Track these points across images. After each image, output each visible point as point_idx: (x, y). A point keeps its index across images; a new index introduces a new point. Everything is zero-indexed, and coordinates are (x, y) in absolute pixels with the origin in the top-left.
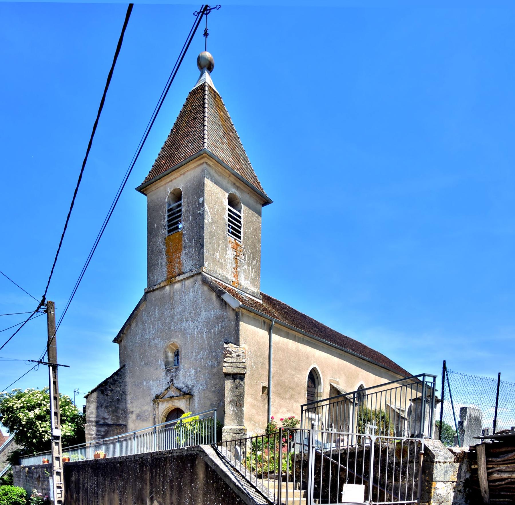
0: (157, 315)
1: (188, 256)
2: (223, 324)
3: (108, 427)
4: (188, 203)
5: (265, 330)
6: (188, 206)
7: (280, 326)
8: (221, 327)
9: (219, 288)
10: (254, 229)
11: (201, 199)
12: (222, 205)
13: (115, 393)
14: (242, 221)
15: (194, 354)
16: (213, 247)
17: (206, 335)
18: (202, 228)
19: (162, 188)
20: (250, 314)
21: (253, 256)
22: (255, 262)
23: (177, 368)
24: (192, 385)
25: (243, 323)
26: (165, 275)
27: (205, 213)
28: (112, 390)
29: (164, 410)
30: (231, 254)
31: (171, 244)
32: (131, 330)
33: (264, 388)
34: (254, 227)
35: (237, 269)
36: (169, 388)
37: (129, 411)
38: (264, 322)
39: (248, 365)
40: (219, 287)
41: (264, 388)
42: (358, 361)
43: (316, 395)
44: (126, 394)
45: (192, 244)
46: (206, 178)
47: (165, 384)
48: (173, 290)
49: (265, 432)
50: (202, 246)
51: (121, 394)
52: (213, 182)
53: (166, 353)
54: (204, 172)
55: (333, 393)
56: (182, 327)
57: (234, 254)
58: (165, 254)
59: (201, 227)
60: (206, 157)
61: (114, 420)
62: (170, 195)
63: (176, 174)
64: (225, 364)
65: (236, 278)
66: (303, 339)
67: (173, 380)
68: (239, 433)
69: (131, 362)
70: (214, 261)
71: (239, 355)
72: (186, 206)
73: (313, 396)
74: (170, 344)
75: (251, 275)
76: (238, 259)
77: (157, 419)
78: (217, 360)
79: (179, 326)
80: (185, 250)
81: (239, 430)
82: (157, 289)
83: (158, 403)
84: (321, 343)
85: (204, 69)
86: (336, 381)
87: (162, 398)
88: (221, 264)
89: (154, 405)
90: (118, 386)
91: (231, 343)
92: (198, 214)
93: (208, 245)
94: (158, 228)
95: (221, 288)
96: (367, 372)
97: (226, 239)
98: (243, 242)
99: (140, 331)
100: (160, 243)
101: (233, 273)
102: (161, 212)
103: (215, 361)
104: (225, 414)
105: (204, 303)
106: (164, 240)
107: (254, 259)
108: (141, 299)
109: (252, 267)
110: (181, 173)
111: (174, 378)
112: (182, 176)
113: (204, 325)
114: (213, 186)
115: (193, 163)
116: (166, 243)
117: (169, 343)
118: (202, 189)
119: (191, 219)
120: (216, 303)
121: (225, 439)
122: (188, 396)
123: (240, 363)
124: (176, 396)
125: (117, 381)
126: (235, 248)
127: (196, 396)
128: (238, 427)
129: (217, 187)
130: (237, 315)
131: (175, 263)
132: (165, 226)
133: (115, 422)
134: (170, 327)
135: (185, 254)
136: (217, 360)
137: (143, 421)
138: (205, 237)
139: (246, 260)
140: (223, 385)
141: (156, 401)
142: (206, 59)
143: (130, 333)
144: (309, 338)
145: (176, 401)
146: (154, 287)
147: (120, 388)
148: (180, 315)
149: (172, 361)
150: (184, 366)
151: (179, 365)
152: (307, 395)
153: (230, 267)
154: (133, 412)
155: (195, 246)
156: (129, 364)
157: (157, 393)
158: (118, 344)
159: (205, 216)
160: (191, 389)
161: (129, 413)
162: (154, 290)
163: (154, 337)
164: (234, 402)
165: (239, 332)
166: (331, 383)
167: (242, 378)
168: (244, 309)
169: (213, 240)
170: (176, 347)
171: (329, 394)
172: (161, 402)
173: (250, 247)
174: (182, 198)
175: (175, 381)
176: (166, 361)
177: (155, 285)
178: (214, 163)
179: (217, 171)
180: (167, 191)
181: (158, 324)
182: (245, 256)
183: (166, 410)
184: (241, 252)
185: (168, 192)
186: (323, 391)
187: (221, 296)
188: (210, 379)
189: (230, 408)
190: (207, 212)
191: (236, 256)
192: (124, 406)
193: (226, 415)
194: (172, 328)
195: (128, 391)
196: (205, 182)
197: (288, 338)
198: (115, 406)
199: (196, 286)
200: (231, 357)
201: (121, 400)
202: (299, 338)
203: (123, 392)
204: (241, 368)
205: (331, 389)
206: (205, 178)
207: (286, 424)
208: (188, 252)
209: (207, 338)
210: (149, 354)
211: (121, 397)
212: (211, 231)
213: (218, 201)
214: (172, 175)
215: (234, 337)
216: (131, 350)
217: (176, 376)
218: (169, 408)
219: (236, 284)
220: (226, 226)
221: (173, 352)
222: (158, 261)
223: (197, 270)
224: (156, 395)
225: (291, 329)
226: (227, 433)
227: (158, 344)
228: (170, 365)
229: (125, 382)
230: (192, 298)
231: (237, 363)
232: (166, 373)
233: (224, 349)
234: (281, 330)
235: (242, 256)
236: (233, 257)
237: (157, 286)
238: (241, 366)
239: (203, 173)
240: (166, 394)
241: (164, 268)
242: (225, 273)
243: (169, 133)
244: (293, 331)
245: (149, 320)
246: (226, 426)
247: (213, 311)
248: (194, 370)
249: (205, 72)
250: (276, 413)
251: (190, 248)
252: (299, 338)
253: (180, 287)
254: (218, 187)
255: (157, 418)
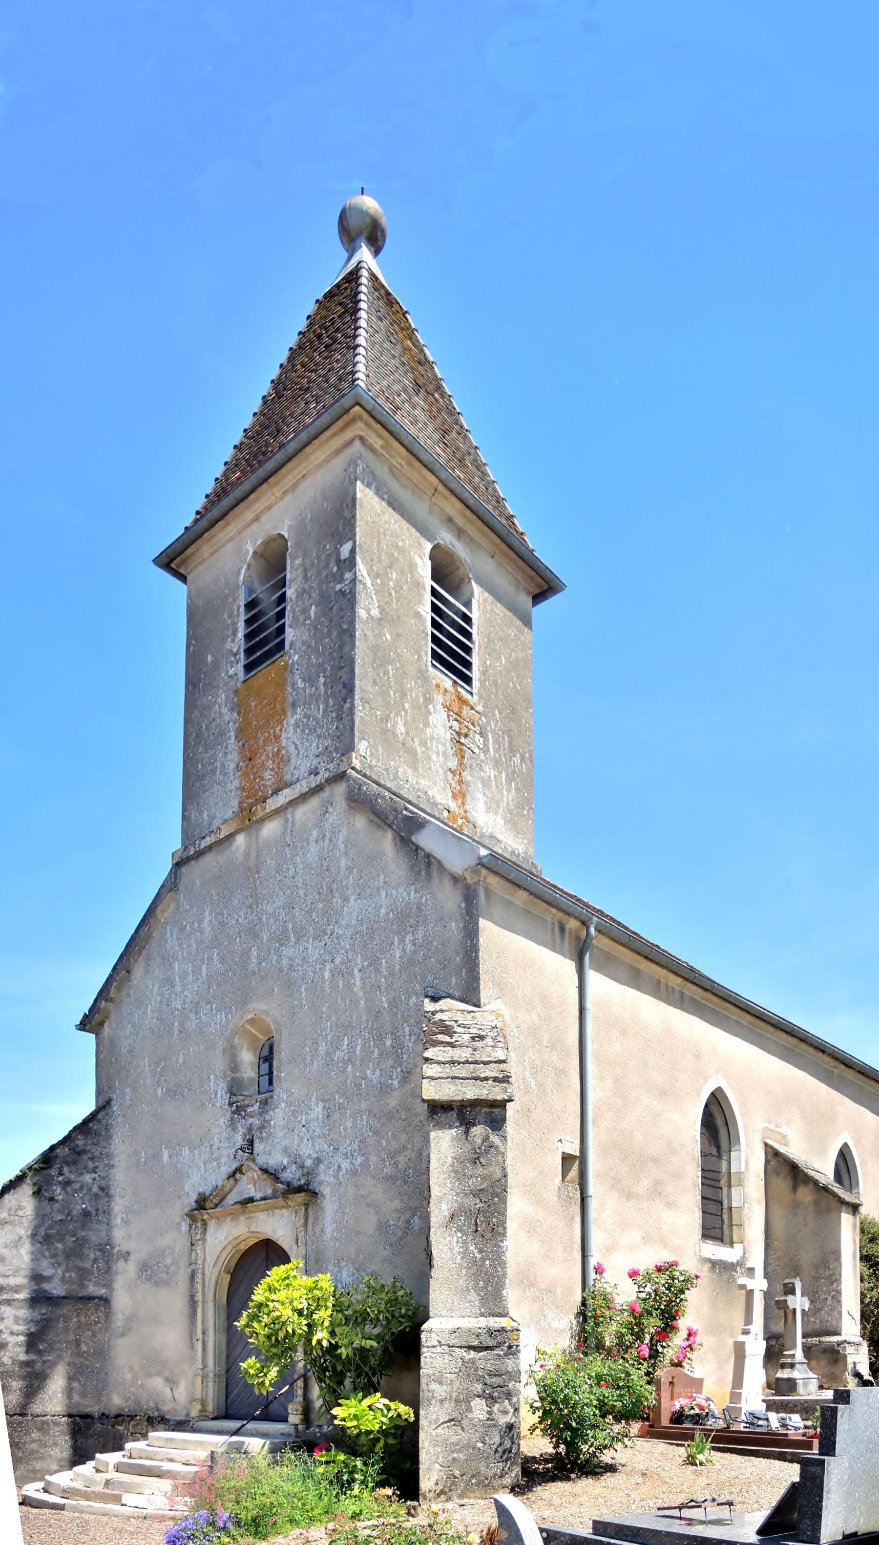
0: (207, 929)
1: (303, 731)
2: (420, 935)
3: (50, 1305)
4: (305, 570)
5: (565, 957)
6: (306, 578)
7: (611, 943)
8: (414, 944)
9: (405, 812)
10: (511, 663)
11: (344, 546)
12: (412, 573)
13: (76, 1191)
14: (474, 631)
15: (322, 1049)
16: (384, 694)
17: (362, 979)
18: (347, 634)
19: (229, 546)
20: (513, 895)
21: (510, 743)
22: (517, 759)
23: (266, 1100)
24: (315, 1156)
25: (490, 924)
26: (235, 803)
27: (359, 587)
28: (67, 1183)
29: (225, 1248)
30: (444, 726)
31: (253, 704)
32: (130, 988)
33: (567, 1159)
34: (510, 654)
35: (463, 774)
36: (239, 1170)
37: (119, 1251)
38: (562, 929)
39: (513, 1069)
40: (406, 809)
41: (567, 1159)
42: (832, 1072)
43: (723, 1183)
44: (112, 1196)
45: (317, 689)
46: (363, 482)
47: (229, 1156)
48: (257, 843)
49: (575, 1322)
50: (349, 688)
51: (96, 1195)
52: (383, 499)
53: (231, 1053)
54: (356, 466)
55: (778, 1174)
56: (285, 962)
57: (451, 727)
58: (236, 737)
59: (346, 631)
60: (361, 419)
61: (70, 1281)
62: (253, 563)
63: (269, 494)
64: (430, 1070)
65: (460, 801)
66: (682, 994)
67: (251, 1142)
68: (487, 1348)
69: (128, 1090)
70: (388, 737)
71: (482, 1038)
72: (300, 578)
73: (713, 1183)
74: (245, 1020)
75: (505, 799)
76: (463, 744)
77: (199, 1279)
78: (401, 1065)
79: (275, 958)
80: (294, 713)
81: (491, 1332)
82: (210, 848)
83: (205, 1223)
84: (733, 1008)
85: (358, 241)
86: (780, 1133)
87: (216, 1206)
88: (412, 752)
89: (193, 1231)
90: (85, 1168)
91: (450, 996)
92: (336, 593)
93: (369, 688)
94: (216, 663)
95: (410, 812)
96: (856, 1105)
97: (425, 678)
98: (481, 697)
99: (156, 988)
100: (220, 707)
101: (451, 785)
102: (226, 615)
103: (393, 1067)
104: (431, 1266)
105: (355, 871)
106: (232, 696)
107: (512, 750)
108: (162, 886)
109: (507, 775)
110: (287, 487)
111: (257, 1134)
112: (288, 498)
113: (354, 946)
114: (384, 513)
115: (321, 445)
116: (238, 705)
117: (242, 1017)
118: (350, 516)
119: (315, 614)
120: (394, 866)
121: (431, 1372)
122: (300, 1197)
123: (485, 1063)
124: (264, 1199)
125: (84, 1152)
126: (456, 710)
127: (328, 1198)
128: (484, 1322)
129: (397, 516)
130: (469, 897)
131: (263, 757)
132: (235, 655)
133: (74, 1287)
134: (245, 965)
135: (296, 726)
136: (401, 1065)
137: (157, 1284)
138: (358, 661)
139: (488, 750)
140: (420, 1154)
141: (199, 1217)
142: (362, 212)
143: (128, 995)
144: (700, 991)
145: (262, 1216)
146: (200, 844)
147: (94, 1175)
148: (277, 920)
149: (253, 1079)
150: (288, 1091)
151: (272, 1091)
152: (703, 1184)
153: (441, 766)
154: (128, 1253)
155: (326, 692)
156: (123, 1094)
157: (201, 1190)
158: (93, 1036)
159: (358, 596)
160: (310, 1173)
161: (118, 1259)
162: (200, 854)
163: (198, 1003)
164: (468, 1218)
165: (477, 957)
166: (768, 1141)
167: (497, 1121)
168: (496, 873)
169: (386, 673)
170: (267, 1030)
171: (763, 1176)
172: (213, 1221)
173: (500, 713)
174: (288, 558)
175: (258, 1147)
176: (233, 1078)
177: (204, 838)
178: (387, 442)
179: (397, 472)
180: (244, 551)
181: (210, 959)
182: (486, 740)
183: (230, 1247)
184: (472, 724)
185: (248, 551)
186: (747, 1169)
187: (413, 839)
188: (376, 1133)
189: (451, 1242)
190: (364, 584)
191: (459, 734)
192: (104, 1234)
193: (434, 1273)
194: (253, 966)
195: (116, 1183)
196: (359, 495)
197: (638, 988)
198: (74, 1236)
199: (331, 820)
200: (451, 1045)
201: (94, 1213)
202: (670, 990)
203: (102, 1189)
204: (490, 1082)
205: (767, 1162)
206: (358, 483)
207: (648, 1289)
208: (306, 716)
209: (364, 988)
210: (181, 1060)
211: (93, 1204)
212: (378, 645)
213: (401, 559)
214: (257, 499)
215: (458, 974)
216: (130, 1052)
217: (262, 1128)
218: (237, 1241)
219: (460, 821)
220: (427, 639)
221: (255, 1049)
222: (216, 761)
223: (331, 766)
224: (199, 1194)
225: (646, 957)
226: (439, 1349)
227: (208, 1025)
228: (245, 1093)
229: (109, 1156)
230: (317, 859)
231: (476, 1062)
232: (232, 1119)
233: (428, 1017)
234: (615, 959)
235: (477, 737)
236: (448, 736)
237: (208, 839)
238: (488, 1074)
239: (351, 469)
240: (231, 1191)
241: (231, 782)
242: (424, 783)
243: (256, 405)
244: (653, 966)
245: (182, 949)
246: (436, 1316)
247: (383, 894)
248: (321, 1105)
249: (361, 246)
250: (609, 1250)
251: (310, 704)
252: (670, 990)
253: (279, 833)
254: (401, 519)
255: (200, 1276)
